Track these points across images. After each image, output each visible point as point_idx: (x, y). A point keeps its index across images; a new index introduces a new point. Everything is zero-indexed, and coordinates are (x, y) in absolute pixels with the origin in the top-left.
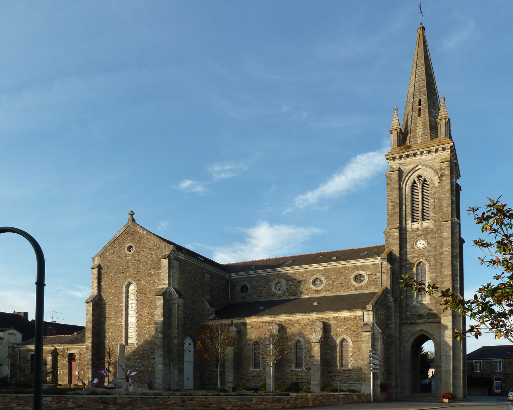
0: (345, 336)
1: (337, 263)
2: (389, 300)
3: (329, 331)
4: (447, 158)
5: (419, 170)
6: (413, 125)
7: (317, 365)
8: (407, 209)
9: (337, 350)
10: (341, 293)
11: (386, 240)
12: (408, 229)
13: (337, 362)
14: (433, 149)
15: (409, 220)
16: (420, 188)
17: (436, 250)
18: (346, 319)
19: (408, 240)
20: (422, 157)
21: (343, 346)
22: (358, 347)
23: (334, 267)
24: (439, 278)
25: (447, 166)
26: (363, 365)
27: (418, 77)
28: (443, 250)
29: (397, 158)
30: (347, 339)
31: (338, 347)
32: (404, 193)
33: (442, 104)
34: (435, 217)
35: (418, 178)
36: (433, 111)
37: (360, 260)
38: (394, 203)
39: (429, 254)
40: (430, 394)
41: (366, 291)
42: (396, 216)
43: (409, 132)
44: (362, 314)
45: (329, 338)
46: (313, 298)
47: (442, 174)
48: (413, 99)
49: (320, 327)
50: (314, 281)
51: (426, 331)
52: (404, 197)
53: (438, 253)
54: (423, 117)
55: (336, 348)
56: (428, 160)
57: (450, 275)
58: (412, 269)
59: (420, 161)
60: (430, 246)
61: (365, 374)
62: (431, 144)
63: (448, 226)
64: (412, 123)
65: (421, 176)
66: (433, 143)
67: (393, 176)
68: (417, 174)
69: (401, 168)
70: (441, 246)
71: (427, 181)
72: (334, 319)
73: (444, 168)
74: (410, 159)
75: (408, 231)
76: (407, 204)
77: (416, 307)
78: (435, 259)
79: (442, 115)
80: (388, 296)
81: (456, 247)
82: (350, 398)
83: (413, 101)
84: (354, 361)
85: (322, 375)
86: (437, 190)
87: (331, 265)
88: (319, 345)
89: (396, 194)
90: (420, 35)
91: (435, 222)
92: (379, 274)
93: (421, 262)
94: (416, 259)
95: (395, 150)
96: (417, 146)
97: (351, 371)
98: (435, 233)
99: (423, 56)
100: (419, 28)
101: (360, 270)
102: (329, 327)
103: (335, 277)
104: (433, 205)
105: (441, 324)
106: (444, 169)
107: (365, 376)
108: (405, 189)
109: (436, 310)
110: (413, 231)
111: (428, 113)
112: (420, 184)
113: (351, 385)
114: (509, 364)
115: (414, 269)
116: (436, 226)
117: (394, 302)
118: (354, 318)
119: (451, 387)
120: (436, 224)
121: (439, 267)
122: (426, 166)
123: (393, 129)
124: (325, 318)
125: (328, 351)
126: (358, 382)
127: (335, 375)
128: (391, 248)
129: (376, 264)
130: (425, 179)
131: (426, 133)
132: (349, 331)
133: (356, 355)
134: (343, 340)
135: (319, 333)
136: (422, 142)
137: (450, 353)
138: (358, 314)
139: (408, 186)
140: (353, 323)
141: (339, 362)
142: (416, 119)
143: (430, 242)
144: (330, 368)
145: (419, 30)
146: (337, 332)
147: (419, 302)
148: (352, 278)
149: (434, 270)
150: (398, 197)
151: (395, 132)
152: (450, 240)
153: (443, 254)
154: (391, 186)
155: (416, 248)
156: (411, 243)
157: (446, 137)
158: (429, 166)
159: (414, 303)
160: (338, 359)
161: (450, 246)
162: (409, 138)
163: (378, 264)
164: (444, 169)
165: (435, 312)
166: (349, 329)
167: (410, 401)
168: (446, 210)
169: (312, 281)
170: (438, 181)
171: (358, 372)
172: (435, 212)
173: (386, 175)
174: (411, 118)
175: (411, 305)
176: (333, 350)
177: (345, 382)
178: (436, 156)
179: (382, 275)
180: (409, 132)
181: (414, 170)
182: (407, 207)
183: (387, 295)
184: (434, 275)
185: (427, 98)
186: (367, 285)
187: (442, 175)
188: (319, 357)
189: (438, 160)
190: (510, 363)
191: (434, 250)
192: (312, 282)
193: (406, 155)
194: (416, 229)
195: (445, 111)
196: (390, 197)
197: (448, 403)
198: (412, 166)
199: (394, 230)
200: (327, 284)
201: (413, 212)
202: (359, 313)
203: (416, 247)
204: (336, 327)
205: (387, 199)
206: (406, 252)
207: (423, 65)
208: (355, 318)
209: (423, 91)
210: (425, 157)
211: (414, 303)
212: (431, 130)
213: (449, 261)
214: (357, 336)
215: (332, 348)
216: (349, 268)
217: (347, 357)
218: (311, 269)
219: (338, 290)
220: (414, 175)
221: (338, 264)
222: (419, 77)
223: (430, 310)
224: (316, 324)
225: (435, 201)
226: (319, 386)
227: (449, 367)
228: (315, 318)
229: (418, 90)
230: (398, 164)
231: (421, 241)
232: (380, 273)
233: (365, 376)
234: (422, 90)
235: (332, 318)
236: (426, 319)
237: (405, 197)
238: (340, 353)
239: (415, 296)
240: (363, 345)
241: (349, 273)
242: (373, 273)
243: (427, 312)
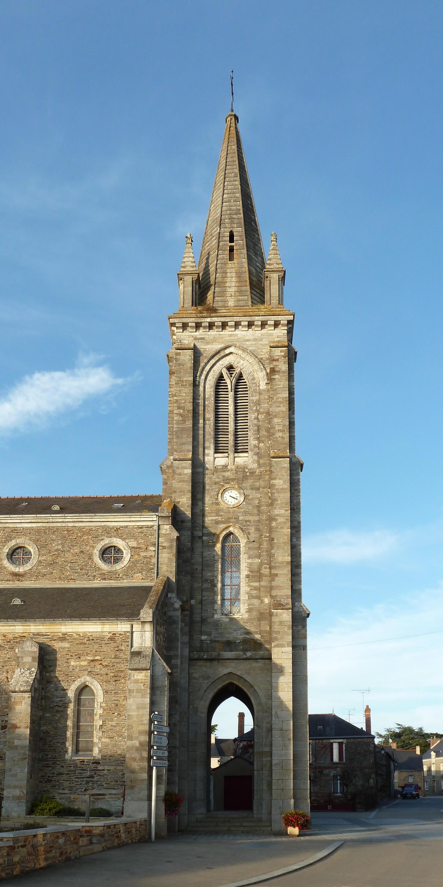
0: (88, 678)
1: (65, 516)
2: (173, 604)
3: (50, 666)
4: (281, 342)
5: (231, 355)
6: (219, 273)
7: (23, 747)
8: (207, 426)
9: (68, 712)
10: (71, 584)
11: (165, 483)
12: (207, 465)
13: (66, 741)
14: (258, 320)
15: (210, 446)
16: (231, 389)
17: (259, 513)
18: (92, 640)
19: (207, 487)
20: (237, 332)
21: (82, 703)
22: (117, 705)
23: (59, 525)
24: (266, 568)
25: (283, 356)
26: (129, 749)
27: (227, 194)
28: (276, 513)
29: (191, 327)
30: (93, 688)
31: (71, 706)
32: (202, 395)
33: (272, 245)
34: (259, 448)
35: (229, 371)
36: (253, 256)
37: (115, 514)
38: (184, 411)
39: (247, 518)
40: (245, 814)
41: (125, 583)
42: (186, 436)
43: (212, 285)
44: (129, 630)
45: (49, 682)
46: (9, 589)
47: (274, 368)
48: (219, 228)
49: (32, 654)
50: (10, 552)
51: (240, 677)
52: (201, 402)
53: (264, 518)
54: (237, 263)
55: (66, 706)
56: (248, 340)
57: (287, 563)
58: (214, 546)
59: (233, 338)
60: (250, 504)
61: (133, 772)
62: (254, 312)
63: (285, 467)
64: (218, 270)
65: (234, 368)
66: (257, 310)
67: (182, 357)
68: (226, 361)
69: (198, 347)
70: (272, 504)
71: (244, 379)
72: (64, 638)
73: (277, 358)
74: (215, 333)
75: (208, 469)
76: (207, 416)
77: (221, 626)
78: (258, 530)
79: (273, 264)
80: (171, 598)
81: (296, 510)
82: (113, 836)
83: (220, 233)
84: (107, 740)
85: (32, 773)
86: (262, 397)
87: (51, 520)
88: (29, 697)
89: (187, 393)
90: (230, 127)
91: (259, 458)
92: (153, 548)
93: (231, 533)
94: (223, 526)
95: (187, 311)
96: (228, 311)
97: (99, 763)
98: (259, 479)
99: (237, 162)
100: (230, 115)
101: (115, 537)
102: (52, 657)
103: (60, 547)
104: (254, 424)
105: (271, 661)
106: (277, 360)
107: (133, 775)
108: (204, 387)
109: (260, 634)
110: (216, 469)
111: (246, 256)
112: (231, 382)
113: (96, 799)
114: (322, 748)
115: (218, 546)
116: (260, 466)
117: (180, 611)
118: (111, 639)
119: (290, 799)
120: (261, 461)
121: (265, 545)
122: (244, 350)
123: (184, 272)
124: (43, 635)
125: (47, 715)
126: (113, 792)
127: (61, 774)
128: (175, 499)
129: (147, 527)
130: (241, 373)
131: (243, 291)
132: (99, 667)
133: (111, 726)
134: (83, 689)
135: (28, 669)
136: (237, 306)
137: (289, 724)
138: (119, 629)
139: (209, 382)
140: (109, 649)
141: (73, 741)
142: (226, 264)
143: (248, 496)
144: (49, 756)
145: (229, 119)
146: (71, 670)
147: (226, 615)
148: (96, 553)
149: (256, 552)
150: (192, 401)
151: (189, 279)
152: (288, 495)
153: (275, 520)
154: (179, 377)
155: (223, 504)
156: (212, 494)
157: (279, 304)
158: (250, 351)
159: (216, 616)
160: (69, 734)
161: (287, 506)
162: (212, 296)
163: (152, 527)
164: (277, 360)
165: (258, 637)
166: (97, 663)
167: (216, 833)
168: (279, 436)
169: (7, 551)
170: (266, 381)
171: (115, 767)
172: (258, 439)
173: (168, 355)
174: (216, 260)
175: (211, 621)
176: (58, 711)
177: (83, 790)
178: (262, 335)
179: (159, 551)
180: (212, 285)
181: (222, 354)
182: (207, 422)
183: (170, 595)
184: (255, 561)
185: (244, 232)
186: (127, 571)
187: (273, 371)
188: (27, 727)
189: (265, 342)
190: (325, 746)
191: (256, 511)
192: (7, 555)
193: (209, 322)
194: (223, 466)
195: (278, 259)
196: (175, 398)
197: (299, 836)
198: (218, 346)
199: (181, 464)
200: (40, 562)
201: (217, 433)
202: (122, 627)
203: (222, 503)
204: (69, 657)
205: (170, 401)
206: (203, 510)
207: (237, 177)
208: (113, 638)
209: (237, 219)
210: (241, 332)
211: (216, 616)
212: (251, 288)
213: (286, 535)
214: (116, 681)
215: (57, 708)
216: (91, 530)
217: (90, 729)
218: (7, 525)
219: (63, 576)
220: (220, 362)
221: (67, 520)
222: (230, 194)
223: (248, 633)
224: (22, 648)
225: (259, 417)
226: (25, 801)
227: (287, 754)
228: (20, 634)
229: (228, 216)
230: (193, 338)
231: (231, 492)
232: (155, 547)
233: (133, 775)
234: (235, 216)
235: (60, 634)
236: (239, 651)
237: (204, 403)
238: (76, 719)
239: (219, 602)
240: (130, 701)
241: (91, 542)
242: (141, 546)
243: (242, 636)
